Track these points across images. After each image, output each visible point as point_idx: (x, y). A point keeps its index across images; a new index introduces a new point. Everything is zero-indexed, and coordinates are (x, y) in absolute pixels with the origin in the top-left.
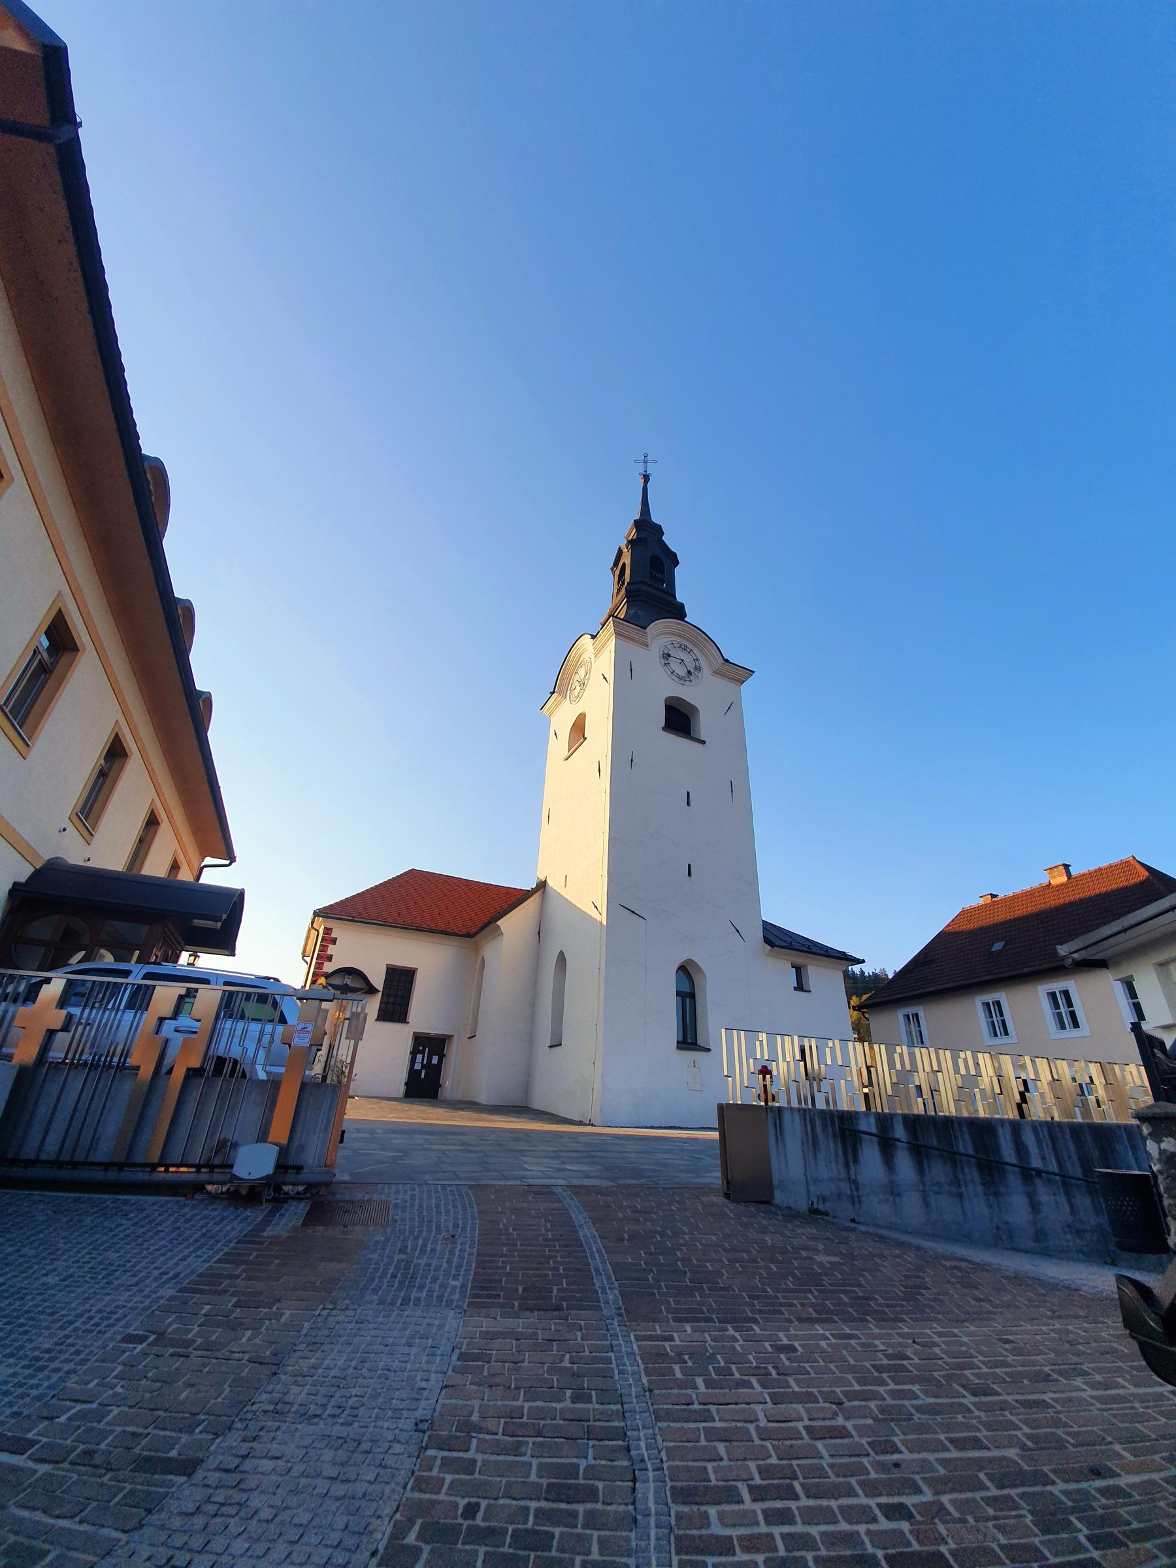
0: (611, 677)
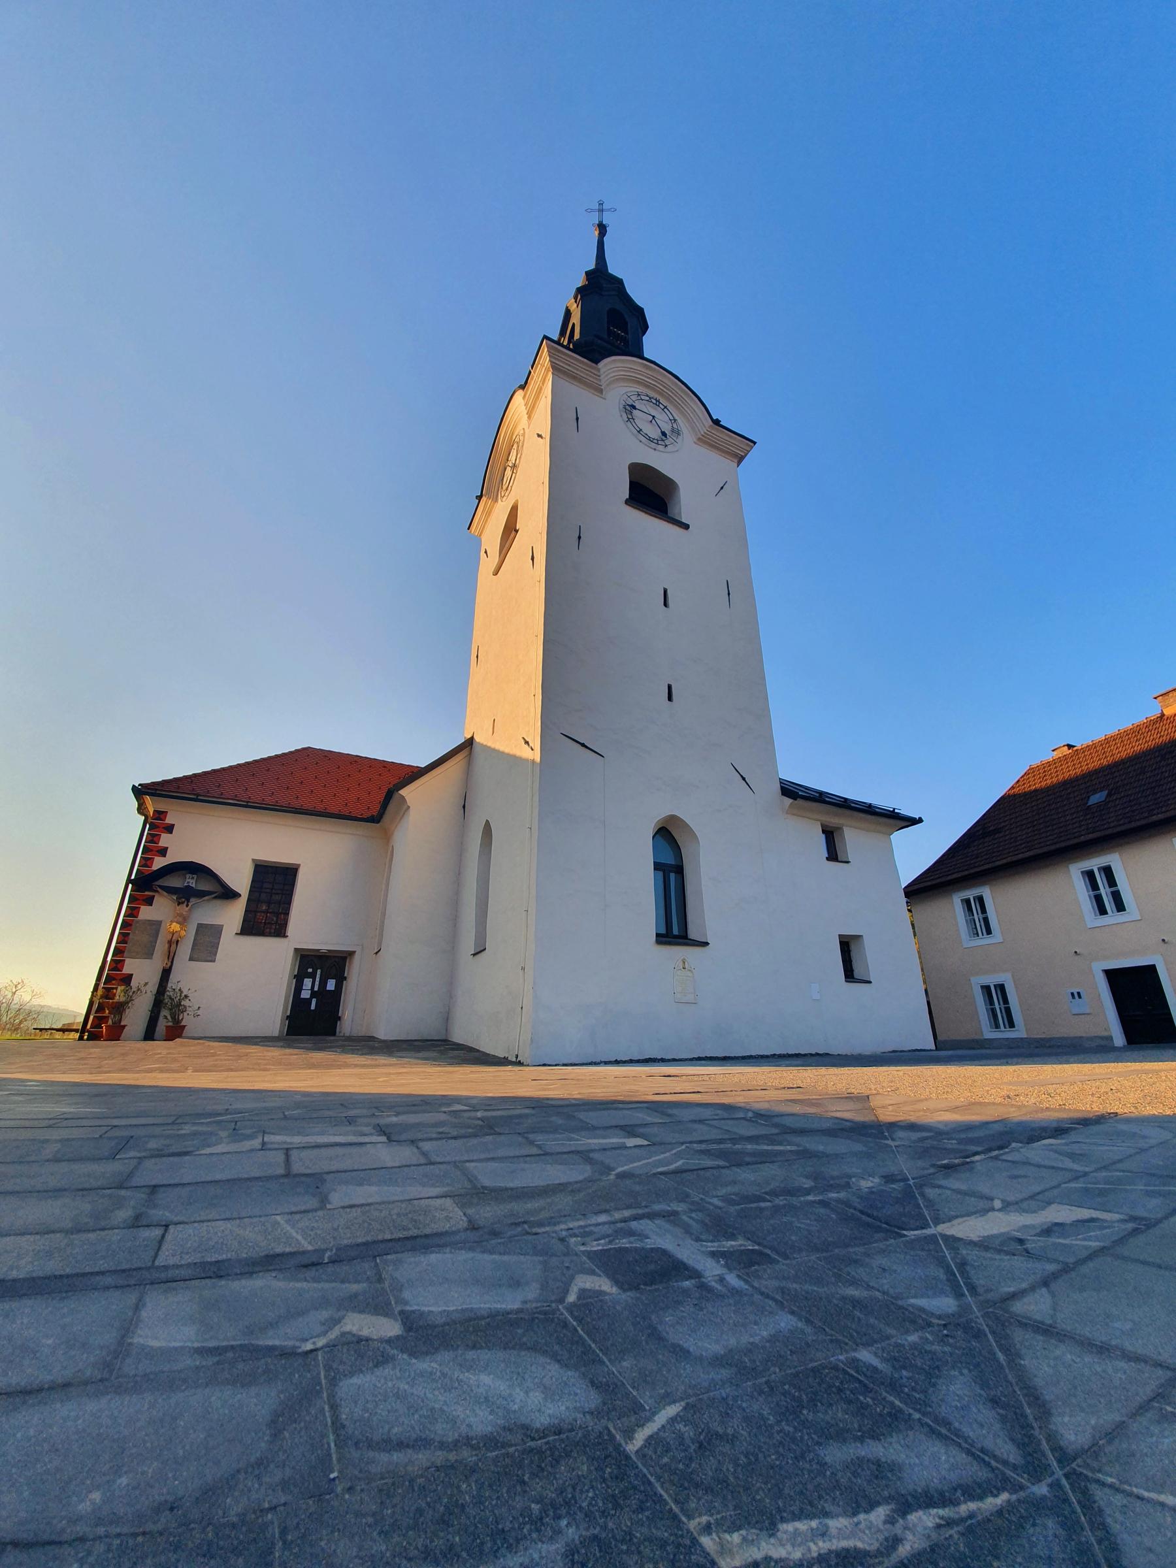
0: (547, 434)
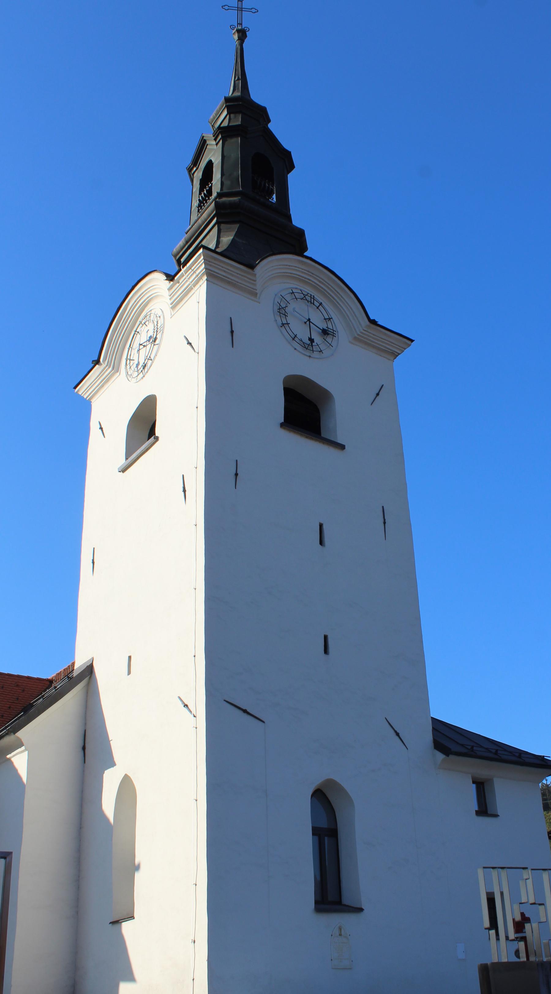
0: (201, 343)
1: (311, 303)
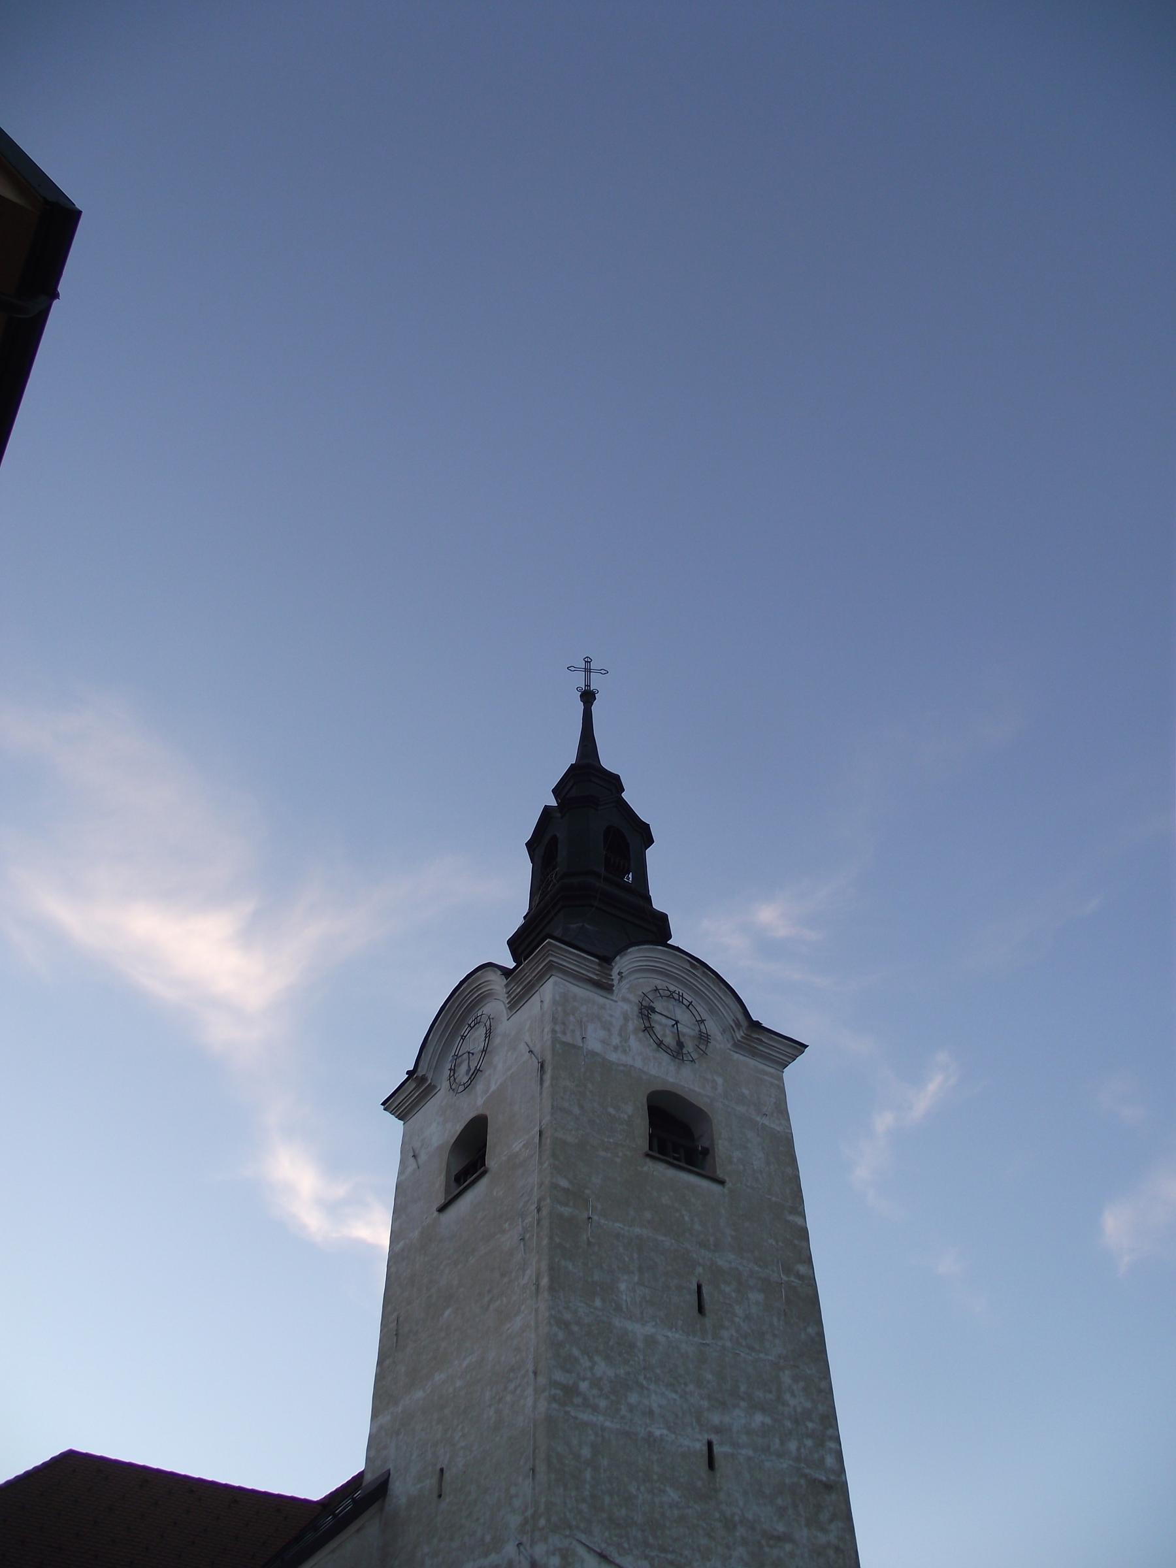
1: (680, 1002)
